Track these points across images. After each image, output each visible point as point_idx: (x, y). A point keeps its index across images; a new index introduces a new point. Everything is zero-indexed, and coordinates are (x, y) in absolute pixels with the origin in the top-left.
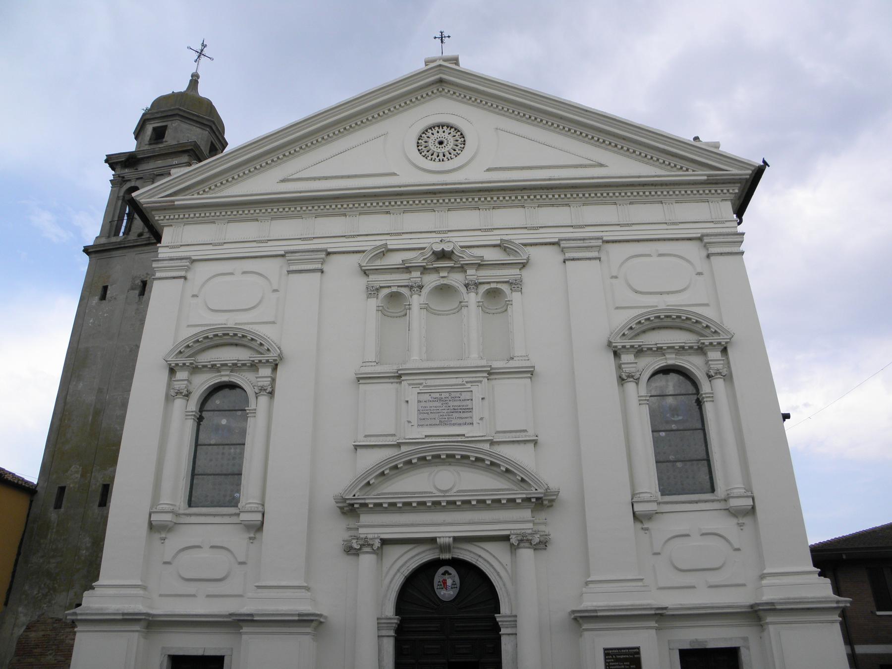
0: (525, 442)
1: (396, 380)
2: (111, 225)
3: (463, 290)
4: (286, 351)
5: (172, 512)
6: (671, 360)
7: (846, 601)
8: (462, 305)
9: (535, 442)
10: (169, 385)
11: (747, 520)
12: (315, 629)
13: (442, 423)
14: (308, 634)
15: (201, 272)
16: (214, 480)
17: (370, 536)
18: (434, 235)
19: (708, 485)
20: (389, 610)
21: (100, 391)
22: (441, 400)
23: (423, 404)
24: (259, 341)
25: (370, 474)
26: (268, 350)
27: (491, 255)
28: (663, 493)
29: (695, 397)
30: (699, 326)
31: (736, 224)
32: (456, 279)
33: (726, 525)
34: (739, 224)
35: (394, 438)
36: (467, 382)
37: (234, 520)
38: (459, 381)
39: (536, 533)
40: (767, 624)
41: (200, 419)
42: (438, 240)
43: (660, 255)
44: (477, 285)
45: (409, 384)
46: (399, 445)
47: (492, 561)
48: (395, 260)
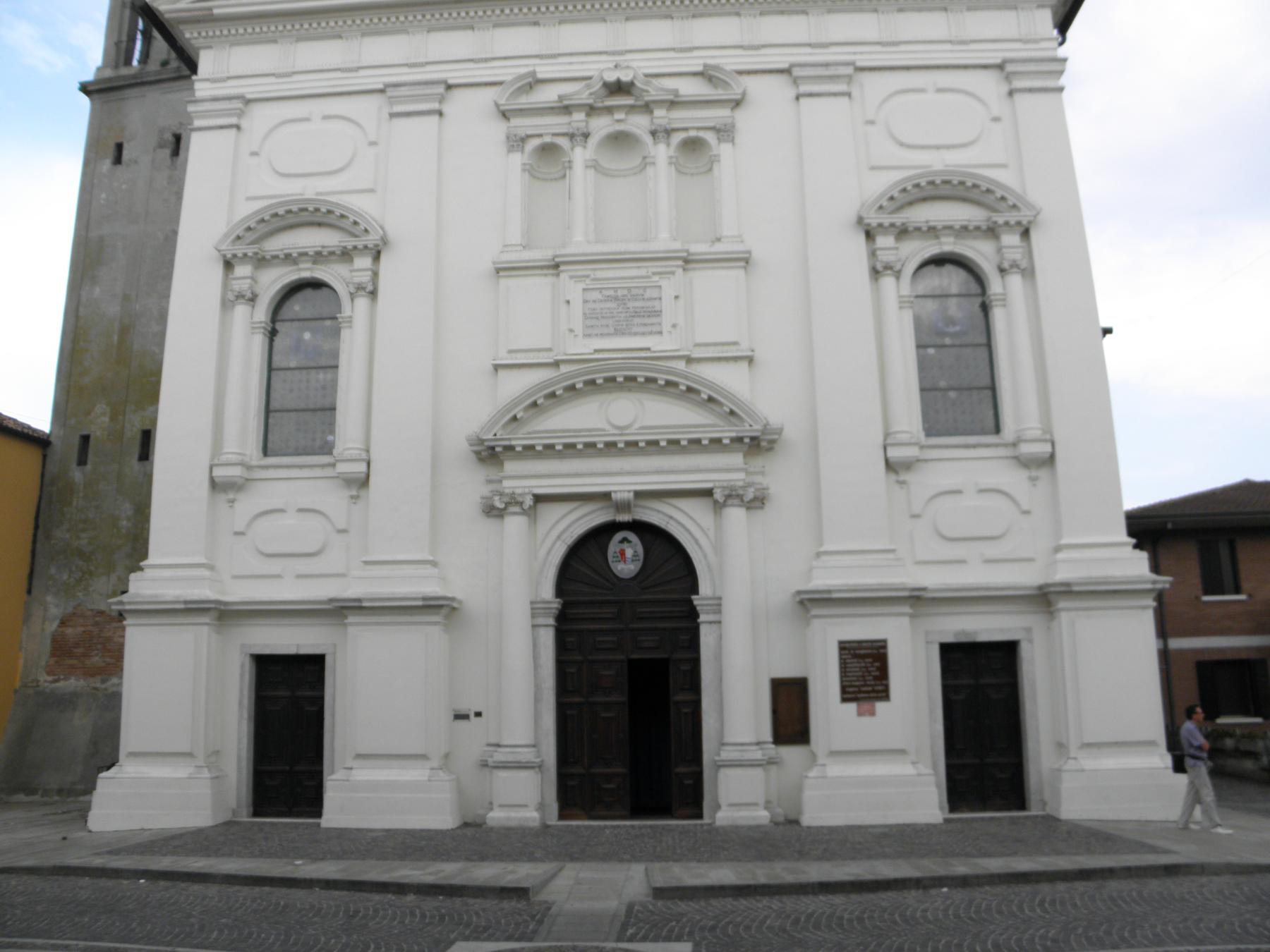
0: (736, 359)
1: (551, 271)
2: (119, 50)
3: (648, 139)
4: (392, 234)
5: (242, 464)
6: (948, 245)
7: (1164, 582)
8: (646, 162)
9: (750, 360)
10: (225, 286)
11: (1043, 473)
12: (447, 617)
13: (619, 332)
14: (435, 623)
15: (260, 118)
16: (297, 417)
17: (518, 491)
18: (604, 58)
19: (990, 422)
20: (547, 591)
21: (126, 298)
22: (616, 298)
23: (591, 305)
24: (352, 218)
25: (516, 405)
26: (366, 231)
27: (690, 88)
28: (929, 432)
29: (979, 300)
30: (991, 197)
31: (1055, 44)
32: (638, 124)
33: (1013, 479)
34: (1062, 43)
35: (551, 354)
36: (654, 274)
37: (329, 472)
38: (643, 272)
39: (749, 485)
40: (1059, 610)
41: (273, 333)
42: (611, 65)
43: (940, 90)
44: (668, 132)
45: (571, 277)
46: (556, 364)
47: (688, 524)
48: (548, 95)
